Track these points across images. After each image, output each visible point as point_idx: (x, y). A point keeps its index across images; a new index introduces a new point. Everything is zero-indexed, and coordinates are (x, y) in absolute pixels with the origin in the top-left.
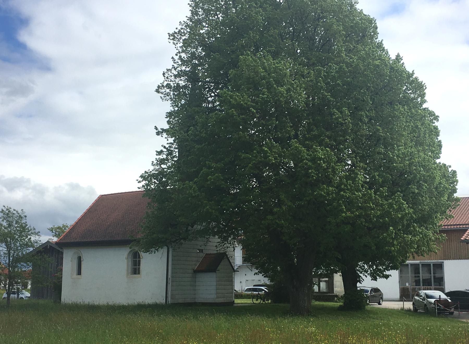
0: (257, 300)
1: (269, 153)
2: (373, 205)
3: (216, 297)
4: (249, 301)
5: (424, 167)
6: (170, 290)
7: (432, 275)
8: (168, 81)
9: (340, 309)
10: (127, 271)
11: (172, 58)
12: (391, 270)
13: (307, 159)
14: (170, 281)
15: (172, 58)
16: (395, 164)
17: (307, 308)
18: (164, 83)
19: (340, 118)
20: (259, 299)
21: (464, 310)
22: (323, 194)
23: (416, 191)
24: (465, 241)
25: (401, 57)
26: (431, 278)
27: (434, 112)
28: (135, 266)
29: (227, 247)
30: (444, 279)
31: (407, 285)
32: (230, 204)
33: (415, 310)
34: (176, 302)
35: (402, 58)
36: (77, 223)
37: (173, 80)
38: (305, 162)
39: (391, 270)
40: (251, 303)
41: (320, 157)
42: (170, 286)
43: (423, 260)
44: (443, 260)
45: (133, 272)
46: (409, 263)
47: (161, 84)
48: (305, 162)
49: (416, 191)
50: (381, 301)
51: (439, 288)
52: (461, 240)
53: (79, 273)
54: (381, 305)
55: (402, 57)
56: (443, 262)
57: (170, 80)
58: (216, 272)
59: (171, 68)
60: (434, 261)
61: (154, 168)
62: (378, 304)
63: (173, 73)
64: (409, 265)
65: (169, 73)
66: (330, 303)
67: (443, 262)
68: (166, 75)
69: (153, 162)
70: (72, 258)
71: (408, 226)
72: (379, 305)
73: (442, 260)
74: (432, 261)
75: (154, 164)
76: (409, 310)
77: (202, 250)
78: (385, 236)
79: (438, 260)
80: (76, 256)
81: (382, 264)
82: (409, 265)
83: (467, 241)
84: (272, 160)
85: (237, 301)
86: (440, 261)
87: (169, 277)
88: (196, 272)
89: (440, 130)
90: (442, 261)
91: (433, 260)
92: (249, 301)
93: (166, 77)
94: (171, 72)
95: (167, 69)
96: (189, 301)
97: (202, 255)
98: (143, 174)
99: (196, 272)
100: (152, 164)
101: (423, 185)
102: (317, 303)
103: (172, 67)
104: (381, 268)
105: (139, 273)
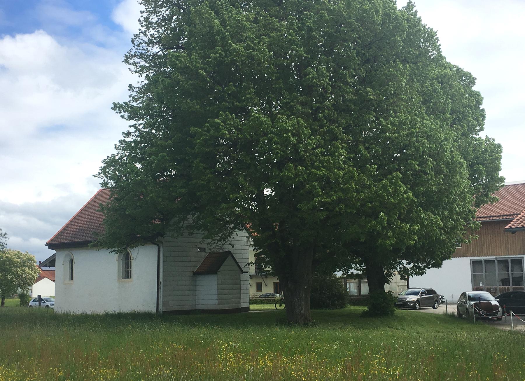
0: (280, 306)
1: (222, 126)
2: (355, 185)
3: (217, 303)
4: (272, 307)
5: (428, 137)
6: (161, 296)
7: (510, 272)
8: (139, 49)
9: (364, 315)
10: (119, 275)
11: (138, 21)
12: (433, 268)
13: (272, 132)
14: (161, 286)
15: (138, 21)
16: (388, 134)
17: (304, 316)
18: (131, 51)
19: (316, 78)
20: (283, 304)
21: (521, 314)
22: (290, 175)
23: (417, 168)
24: (510, 229)
25: (413, 3)
26: (509, 278)
27: (470, 74)
28: (475, 274)
29: (223, 245)
30: (69, 269)
31: (481, 285)
32: (180, 190)
33: (460, 315)
34: (170, 309)
35: (415, 5)
36: (71, 221)
37: (145, 48)
38: (270, 136)
39: (433, 268)
40: (274, 309)
41: (286, 128)
42: (161, 291)
43: (499, 256)
44: (523, 255)
45: (125, 276)
46: (483, 259)
47: (128, 52)
48: (270, 136)
49: (417, 168)
50: (436, 305)
51: (518, 288)
52: (506, 229)
53: (72, 279)
54: (437, 309)
55: (414, 3)
56: (523, 257)
57: (141, 48)
58: (217, 274)
59: (138, 34)
60: (512, 256)
61: (118, 152)
62: (432, 308)
63: (142, 39)
64: (483, 262)
65: (138, 39)
66: (358, 307)
67: (523, 257)
68: (136, 43)
69: (116, 145)
70: (64, 262)
71: (410, 211)
72: (433, 309)
73: (521, 255)
74: (510, 257)
75: (117, 147)
76: (452, 316)
77: (205, 248)
78: (373, 225)
79: (517, 255)
80: (68, 260)
81: (422, 261)
82: (483, 262)
83: (512, 229)
84: (226, 134)
85: (252, 307)
86: (519, 256)
87: (161, 280)
88: (196, 274)
89: (483, 98)
90: (522, 256)
91: (511, 255)
92: (272, 307)
93: (136, 44)
94: (139, 39)
95: (134, 35)
96: (187, 308)
97: (203, 254)
98: (105, 160)
99: (196, 274)
100: (115, 147)
101: (428, 160)
102: (352, 308)
103: (139, 31)
104: (421, 266)
105: (131, 278)
